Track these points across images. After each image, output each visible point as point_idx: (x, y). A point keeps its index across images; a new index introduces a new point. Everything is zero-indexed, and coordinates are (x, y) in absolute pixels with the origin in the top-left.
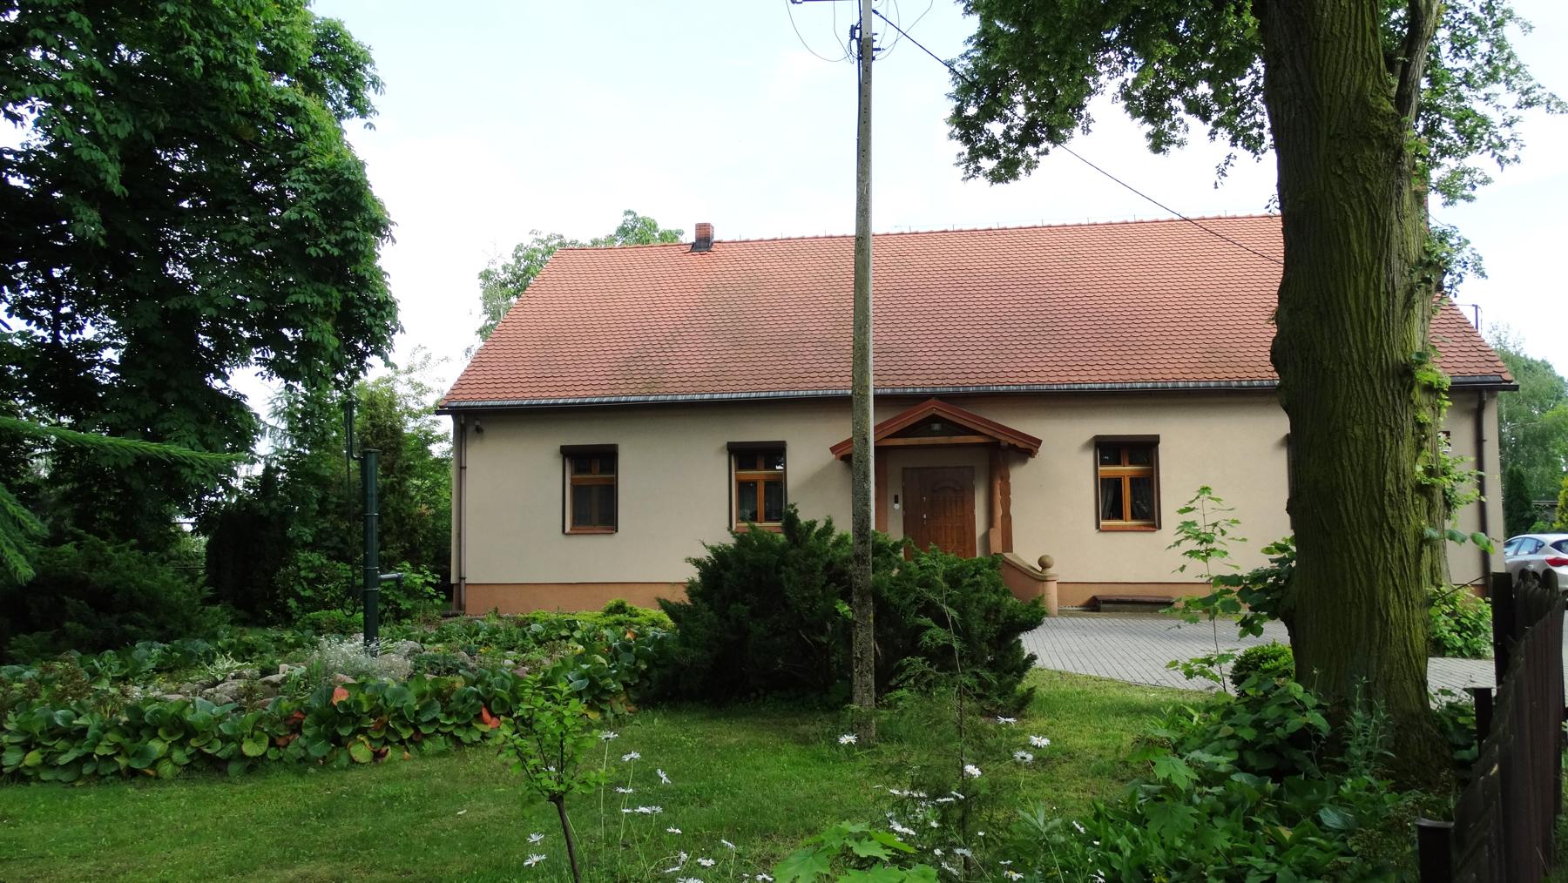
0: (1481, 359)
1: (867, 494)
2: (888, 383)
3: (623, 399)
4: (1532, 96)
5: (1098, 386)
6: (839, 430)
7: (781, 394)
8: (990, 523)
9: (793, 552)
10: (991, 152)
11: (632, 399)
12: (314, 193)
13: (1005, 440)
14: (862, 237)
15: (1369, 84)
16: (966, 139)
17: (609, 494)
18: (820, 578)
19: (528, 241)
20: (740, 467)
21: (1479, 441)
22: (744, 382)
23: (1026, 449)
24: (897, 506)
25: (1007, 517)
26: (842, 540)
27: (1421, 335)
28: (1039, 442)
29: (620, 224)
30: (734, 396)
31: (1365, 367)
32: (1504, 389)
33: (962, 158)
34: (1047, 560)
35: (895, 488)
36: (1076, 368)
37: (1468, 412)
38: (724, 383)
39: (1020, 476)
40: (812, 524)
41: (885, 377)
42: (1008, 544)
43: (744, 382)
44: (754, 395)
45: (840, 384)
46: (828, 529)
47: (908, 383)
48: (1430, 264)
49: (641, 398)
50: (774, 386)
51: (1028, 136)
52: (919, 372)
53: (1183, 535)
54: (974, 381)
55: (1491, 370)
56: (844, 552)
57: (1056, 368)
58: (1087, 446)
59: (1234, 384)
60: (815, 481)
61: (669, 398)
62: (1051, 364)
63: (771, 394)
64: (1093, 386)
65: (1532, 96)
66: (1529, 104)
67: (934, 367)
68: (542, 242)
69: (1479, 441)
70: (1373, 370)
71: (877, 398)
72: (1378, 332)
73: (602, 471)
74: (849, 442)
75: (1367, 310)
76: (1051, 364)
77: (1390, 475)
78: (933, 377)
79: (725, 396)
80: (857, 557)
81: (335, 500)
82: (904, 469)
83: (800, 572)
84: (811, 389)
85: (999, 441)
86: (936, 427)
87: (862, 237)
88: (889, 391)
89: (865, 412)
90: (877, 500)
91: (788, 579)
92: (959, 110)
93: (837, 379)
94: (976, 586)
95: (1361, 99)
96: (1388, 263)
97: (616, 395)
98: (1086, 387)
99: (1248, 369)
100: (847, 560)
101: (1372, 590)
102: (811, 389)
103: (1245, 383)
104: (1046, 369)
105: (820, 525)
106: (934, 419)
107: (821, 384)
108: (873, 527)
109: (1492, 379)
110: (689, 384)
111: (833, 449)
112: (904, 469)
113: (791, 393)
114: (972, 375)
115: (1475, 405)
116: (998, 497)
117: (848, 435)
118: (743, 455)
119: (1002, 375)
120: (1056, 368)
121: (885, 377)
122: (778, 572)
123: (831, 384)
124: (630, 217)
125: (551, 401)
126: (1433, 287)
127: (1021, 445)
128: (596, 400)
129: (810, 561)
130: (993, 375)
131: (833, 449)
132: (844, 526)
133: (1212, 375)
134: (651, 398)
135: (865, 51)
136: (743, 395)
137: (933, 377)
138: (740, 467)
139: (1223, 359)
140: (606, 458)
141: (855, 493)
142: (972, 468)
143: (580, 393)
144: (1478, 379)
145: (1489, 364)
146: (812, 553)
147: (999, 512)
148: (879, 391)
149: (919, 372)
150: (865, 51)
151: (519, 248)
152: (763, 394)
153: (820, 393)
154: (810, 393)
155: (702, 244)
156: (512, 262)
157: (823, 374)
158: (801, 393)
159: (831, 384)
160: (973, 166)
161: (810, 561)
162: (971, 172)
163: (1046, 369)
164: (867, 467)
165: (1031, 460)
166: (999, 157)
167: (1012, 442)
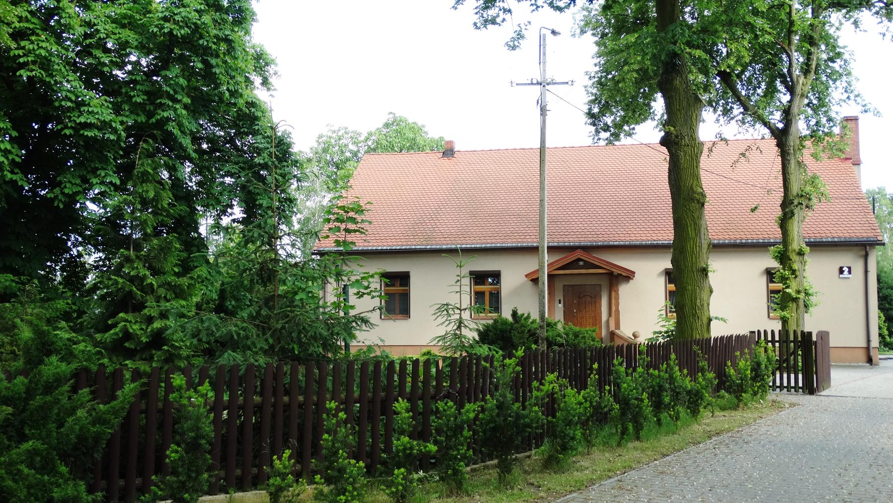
0: (869, 228)
1: (544, 304)
2: (555, 239)
3: (413, 247)
4: (867, 108)
5: (666, 242)
6: (529, 264)
7: (498, 245)
8: (610, 315)
9: (515, 325)
10: (606, 128)
11: (418, 247)
12: (268, 148)
13: (616, 272)
14: (542, 149)
15: (695, 183)
16: (594, 124)
17: (405, 298)
18: (526, 335)
19: (325, 132)
20: (476, 284)
21: (866, 272)
22: (478, 238)
23: (627, 276)
24: (560, 305)
25: (617, 311)
26: (534, 322)
27: (797, 229)
28: (634, 273)
29: (385, 121)
30: (473, 246)
31: (692, 268)
32: (878, 244)
33: (591, 134)
34: (637, 334)
35: (559, 295)
36: (656, 232)
37: (861, 256)
38: (468, 238)
39: (624, 290)
40: (523, 315)
41: (554, 236)
42: (618, 326)
43: (478, 238)
44: (483, 246)
45: (529, 240)
46: (528, 317)
47: (566, 240)
48: (802, 196)
49: (423, 247)
50: (494, 241)
51: (625, 121)
52: (572, 233)
53: (661, 319)
54: (601, 240)
55: (872, 234)
56: (535, 326)
57: (645, 232)
58: (660, 274)
59: (738, 241)
60: (517, 291)
61: (438, 247)
62: (643, 229)
63: (493, 245)
64: (664, 242)
65: (867, 108)
66: (866, 111)
67: (581, 230)
68: (334, 132)
69: (866, 272)
70: (694, 269)
71: (549, 248)
72: (696, 258)
73: (400, 286)
74: (536, 271)
75: (693, 251)
76: (643, 229)
77: (698, 300)
78: (580, 236)
79: (468, 246)
80: (540, 327)
81: (256, 300)
82: (564, 286)
83: (518, 333)
84: (514, 242)
85: (613, 272)
86: (581, 263)
87: (542, 149)
88: (556, 244)
89: (543, 257)
90: (549, 294)
91: (514, 335)
92: (590, 109)
93: (528, 237)
94: (584, 338)
95: (692, 188)
96: (700, 237)
97: (409, 245)
98: (660, 242)
99: (747, 233)
100: (536, 329)
101: (692, 335)
102: (514, 242)
103: (744, 241)
104: (640, 232)
105: (526, 315)
106: (579, 260)
107: (520, 240)
108: (546, 316)
109: (872, 239)
110: (448, 239)
111: (526, 276)
112: (564, 286)
113: (504, 245)
114: (601, 236)
115: (864, 253)
116: (613, 301)
117: (537, 267)
118: (479, 277)
119: (617, 235)
120: (645, 232)
121: (554, 236)
122: (510, 333)
123: (525, 240)
124: (392, 116)
125: (374, 248)
126: (804, 206)
127: (624, 274)
128: (398, 248)
129: (522, 329)
130: (612, 236)
131: (526, 276)
132: (535, 316)
133: (727, 236)
134: (428, 247)
135: (543, 111)
136: (478, 246)
137: (580, 236)
138: (476, 284)
139: (735, 227)
140: (403, 279)
141: (540, 303)
142: (600, 285)
143: (390, 244)
144: (865, 239)
145: (873, 231)
146: (523, 326)
147: (614, 309)
148: (550, 244)
149: (572, 233)
150: (543, 111)
151: (320, 137)
152: (489, 245)
153: (519, 245)
154: (514, 245)
155: (449, 152)
156: (316, 145)
157: (521, 234)
158: (509, 245)
159: (525, 240)
160: (596, 138)
161: (522, 329)
162: (595, 141)
163: (640, 232)
164: (544, 294)
165: (631, 281)
166: (610, 131)
167: (619, 272)
